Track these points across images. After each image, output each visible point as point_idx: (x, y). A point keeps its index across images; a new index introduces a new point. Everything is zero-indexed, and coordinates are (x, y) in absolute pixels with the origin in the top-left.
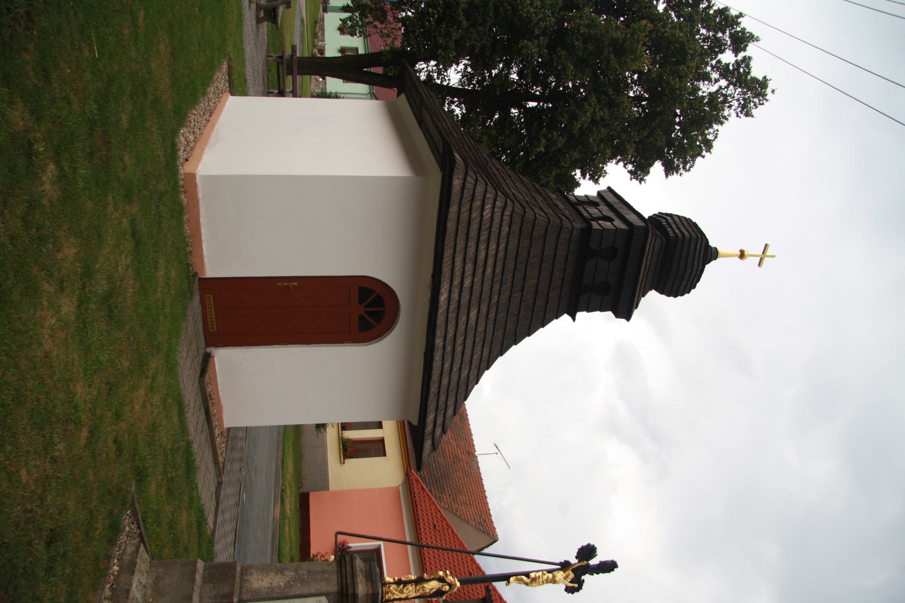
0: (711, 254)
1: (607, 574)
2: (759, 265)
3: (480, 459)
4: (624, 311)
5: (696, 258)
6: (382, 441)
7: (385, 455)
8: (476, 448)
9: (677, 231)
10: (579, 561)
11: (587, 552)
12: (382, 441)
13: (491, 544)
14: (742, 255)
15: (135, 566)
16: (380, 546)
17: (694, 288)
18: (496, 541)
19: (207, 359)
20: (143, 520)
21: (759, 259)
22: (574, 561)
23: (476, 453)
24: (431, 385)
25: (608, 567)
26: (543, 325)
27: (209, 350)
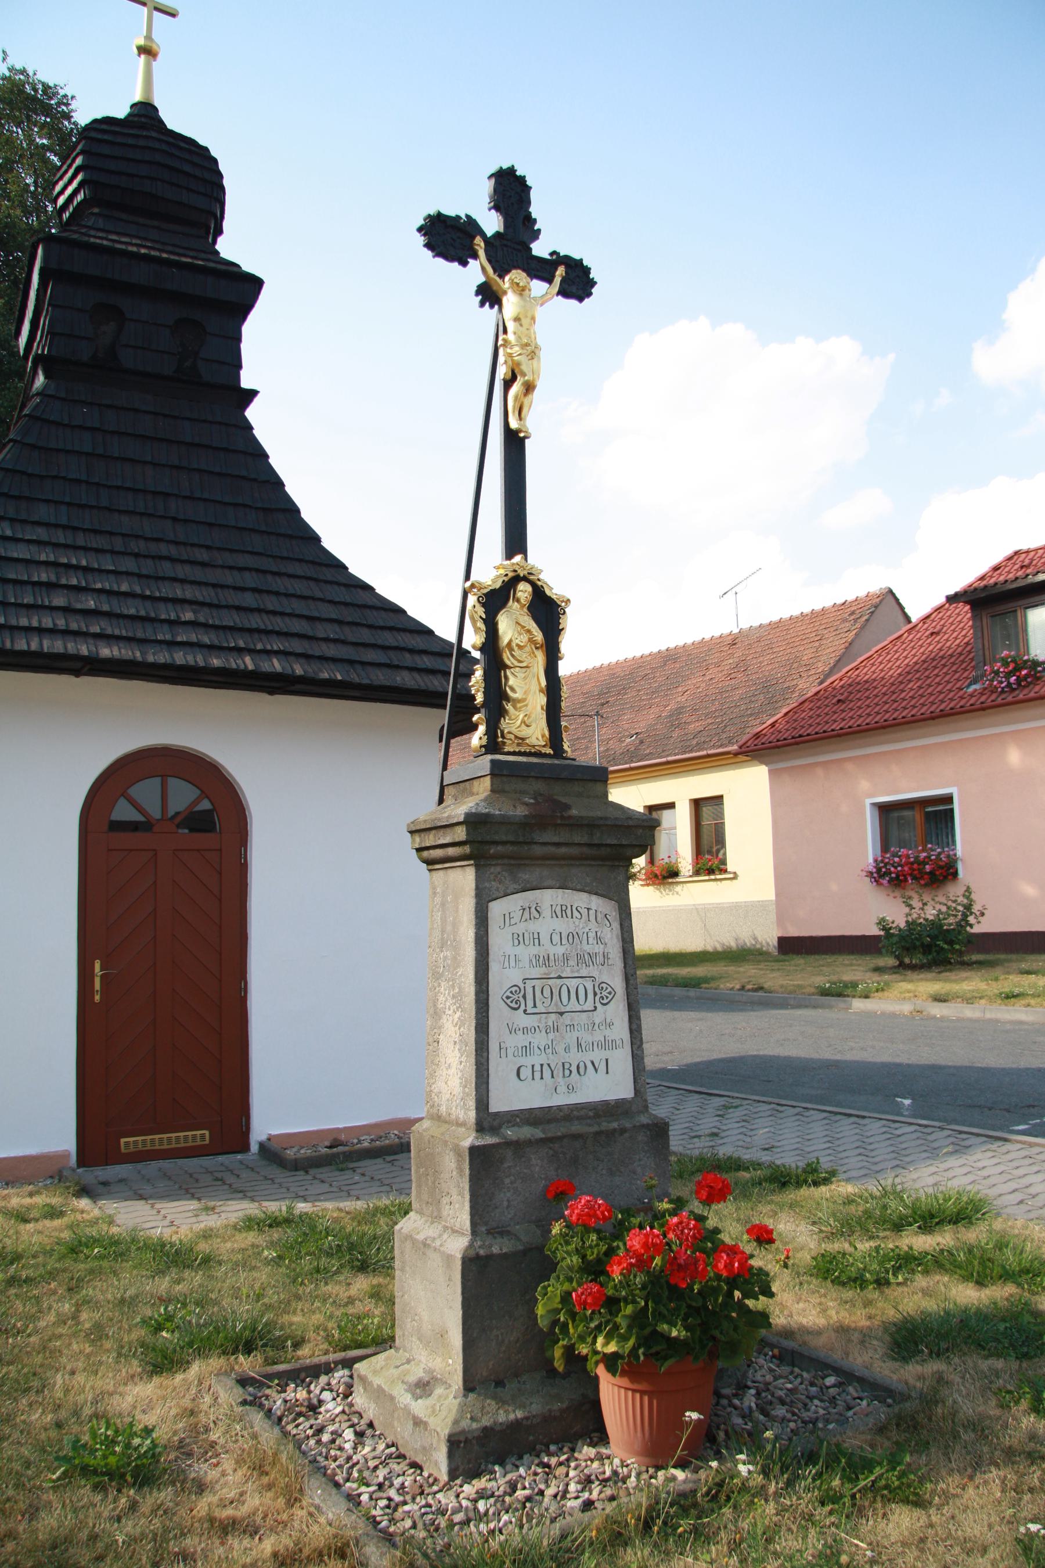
0: (145, 113)
1: (533, 195)
2: (173, 15)
3: (745, 625)
4: (244, 289)
5: (131, 141)
6: (697, 804)
7: (721, 797)
8: (726, 631)
9: (75, 184)
10: (475, 256)
11: (447, 236)
12: (697, 804)
13: (897, 600)
14: (147, 51)
15: (383, 1391)
16: (874, 804)
17: (206, 149)
18: (891, 592)
19: (271, 1153)
20: (345, 1348)
21: (155, 13)
22: (475, 272)
23: (736, 631)
24: (431, 688)
25: (510, 190)
26: (262, 455)
27: (254, 1148)
